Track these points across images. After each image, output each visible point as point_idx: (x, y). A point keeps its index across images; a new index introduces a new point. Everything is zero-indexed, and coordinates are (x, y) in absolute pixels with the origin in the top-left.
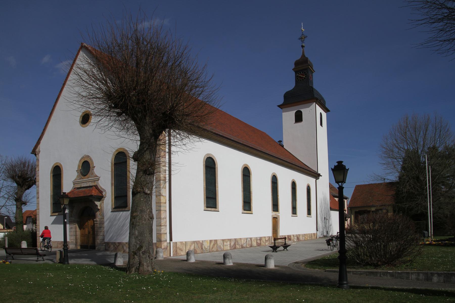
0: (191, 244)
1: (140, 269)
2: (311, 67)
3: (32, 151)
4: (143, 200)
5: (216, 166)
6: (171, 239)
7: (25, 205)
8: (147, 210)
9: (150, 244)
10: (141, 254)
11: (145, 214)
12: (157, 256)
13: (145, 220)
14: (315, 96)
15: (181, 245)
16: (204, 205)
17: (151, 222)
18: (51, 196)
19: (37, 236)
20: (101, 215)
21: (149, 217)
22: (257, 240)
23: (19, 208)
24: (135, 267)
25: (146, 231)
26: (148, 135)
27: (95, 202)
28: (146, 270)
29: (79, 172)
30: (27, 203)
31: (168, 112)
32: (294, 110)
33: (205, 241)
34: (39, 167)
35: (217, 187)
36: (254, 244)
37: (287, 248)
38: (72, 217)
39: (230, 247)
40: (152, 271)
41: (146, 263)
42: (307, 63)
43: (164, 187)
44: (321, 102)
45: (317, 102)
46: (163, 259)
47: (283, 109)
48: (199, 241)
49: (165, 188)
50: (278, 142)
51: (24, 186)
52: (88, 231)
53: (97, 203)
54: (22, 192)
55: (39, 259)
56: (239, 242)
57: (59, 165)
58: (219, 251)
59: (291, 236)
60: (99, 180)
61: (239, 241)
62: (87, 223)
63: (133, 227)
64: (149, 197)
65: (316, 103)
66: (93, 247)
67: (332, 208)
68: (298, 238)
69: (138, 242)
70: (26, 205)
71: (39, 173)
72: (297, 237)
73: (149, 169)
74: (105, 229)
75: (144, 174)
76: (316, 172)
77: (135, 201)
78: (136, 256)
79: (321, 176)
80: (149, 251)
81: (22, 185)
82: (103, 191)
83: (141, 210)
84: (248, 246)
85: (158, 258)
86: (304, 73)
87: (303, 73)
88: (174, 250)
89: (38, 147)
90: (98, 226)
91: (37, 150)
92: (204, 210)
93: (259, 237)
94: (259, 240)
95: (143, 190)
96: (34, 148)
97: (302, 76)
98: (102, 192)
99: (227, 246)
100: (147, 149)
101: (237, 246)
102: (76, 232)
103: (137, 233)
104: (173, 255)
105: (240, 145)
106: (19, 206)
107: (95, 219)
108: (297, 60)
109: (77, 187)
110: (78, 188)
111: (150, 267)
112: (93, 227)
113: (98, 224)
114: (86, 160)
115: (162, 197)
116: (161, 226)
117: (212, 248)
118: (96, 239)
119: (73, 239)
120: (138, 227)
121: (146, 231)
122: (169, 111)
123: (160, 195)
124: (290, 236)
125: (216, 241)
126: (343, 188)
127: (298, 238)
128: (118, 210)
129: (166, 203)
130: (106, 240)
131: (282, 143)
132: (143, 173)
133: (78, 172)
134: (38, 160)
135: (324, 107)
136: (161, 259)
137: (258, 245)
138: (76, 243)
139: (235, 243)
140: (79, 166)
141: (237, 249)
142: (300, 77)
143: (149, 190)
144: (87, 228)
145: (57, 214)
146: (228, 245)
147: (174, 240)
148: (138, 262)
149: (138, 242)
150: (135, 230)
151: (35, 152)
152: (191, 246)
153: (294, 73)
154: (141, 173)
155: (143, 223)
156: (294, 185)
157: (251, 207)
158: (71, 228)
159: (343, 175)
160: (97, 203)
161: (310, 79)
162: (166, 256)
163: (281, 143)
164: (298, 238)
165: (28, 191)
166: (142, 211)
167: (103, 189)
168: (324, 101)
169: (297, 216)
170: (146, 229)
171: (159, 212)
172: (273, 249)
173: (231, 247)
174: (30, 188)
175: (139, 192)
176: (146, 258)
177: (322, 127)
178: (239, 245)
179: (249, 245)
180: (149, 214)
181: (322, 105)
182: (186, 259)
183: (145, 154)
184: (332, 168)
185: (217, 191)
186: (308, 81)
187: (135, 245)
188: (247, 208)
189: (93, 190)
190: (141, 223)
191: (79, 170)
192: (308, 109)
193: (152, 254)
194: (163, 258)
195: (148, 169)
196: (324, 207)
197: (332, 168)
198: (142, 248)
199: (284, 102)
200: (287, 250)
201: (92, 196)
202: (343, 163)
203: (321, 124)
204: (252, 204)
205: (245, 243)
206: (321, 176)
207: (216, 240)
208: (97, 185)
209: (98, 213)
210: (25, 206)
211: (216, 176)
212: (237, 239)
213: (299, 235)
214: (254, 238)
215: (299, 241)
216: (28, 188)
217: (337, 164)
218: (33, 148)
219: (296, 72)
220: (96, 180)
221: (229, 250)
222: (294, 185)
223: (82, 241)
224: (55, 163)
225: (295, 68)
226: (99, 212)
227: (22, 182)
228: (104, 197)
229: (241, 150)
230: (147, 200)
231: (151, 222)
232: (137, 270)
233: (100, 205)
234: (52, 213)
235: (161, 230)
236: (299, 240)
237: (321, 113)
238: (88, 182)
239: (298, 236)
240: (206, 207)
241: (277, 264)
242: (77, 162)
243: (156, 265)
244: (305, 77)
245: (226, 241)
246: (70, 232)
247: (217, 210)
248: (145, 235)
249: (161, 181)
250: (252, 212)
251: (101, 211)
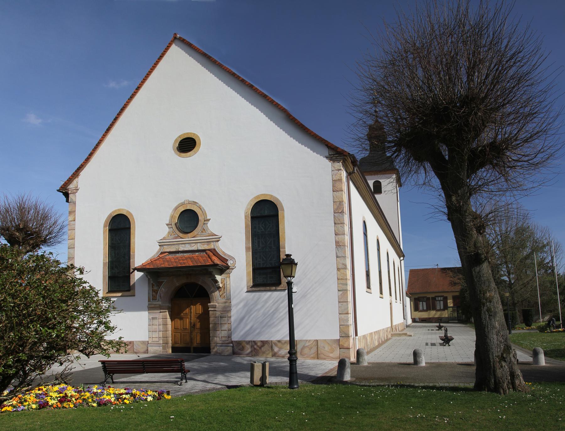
6: (356, 335)
18: (104, 264)
27: (216, 276)
52: (190, 323)
53: (218, 278)
60: (218, 241)
62: (187, 310)
74: (232, 319)
82: (228, 259)
91: (71, 186)
102: (165, 324)
112: (205, 317)
123: (345, 267)
126: (292, 283)
128: (258, 289)
130: (235, 337)
133: (170, 226)
140: (172, 217)
145: (120, 294)
159: (291, 268)
167: (229, 256)
191: (173, 224)
202: (292, 257)
208: (215, 249)
218: (62, 183)
223: (174, 342)
234: (107, 293)
238: (194, 244)
242: (170, 211)
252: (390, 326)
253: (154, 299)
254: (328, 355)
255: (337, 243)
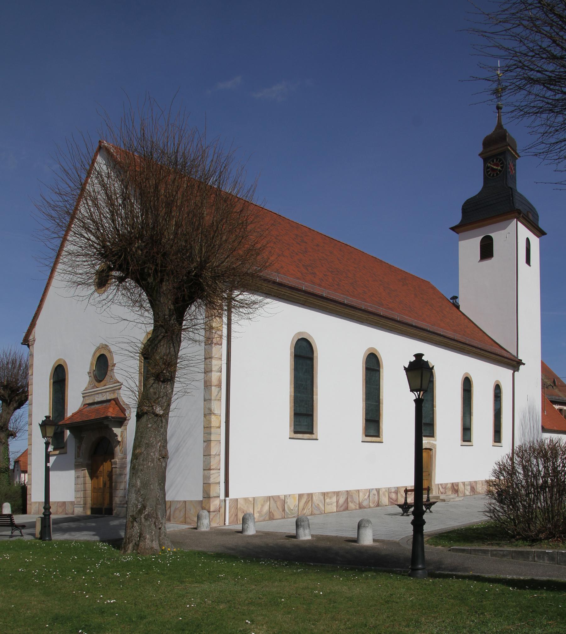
0: (264, 502)
1: (140, 545)
2: (511, 148)
3: (23, 339)
4: (151, 427)
5: (315, 355)
6: (227, 495)
7: (13, 438)
8: (156, 444)
9: (159, 502)
10: (143, 520)
11: (153, 450)
12: (199, 524)
13: (153, 461)
14: (517, 206)
15: (246, 504)
16: (290, 428)
17: (163, 464)
19: (28, 493)
20: (123, 451)
21: (160, 455)
22: (391, 492)
23: (4, 443)
24: (134, 542)
25: (154, 479)
26: (167, 312)
27: (114, 429)
28: (148, 547)
29: (92, 375)
30: (17, 434)
31: (193, 272)
32: (481, 236)
33: (290, 495)
34: (33, 369)
35: (314, 393)
36: (385, 500)
37: (430, 507)
38: (79, 457)
39: (337, 506)
40: (158, 548)
41: (150, 535)
42: (505, 139)
43: (218, 398)
44: (529, 218)
45: (519, 217)
46: (208, 530)
47: (459, 234)
48: (279, 497)
49: (220, 400)
50: (451, 299)
51: (12, 403)
52: (103, 481)
53: (117, 431)
54: (8, 413)
55: (14, 534)
56: (355, 496)
57: (62, 364)
58: (315, 514)
59: (458, 485)
60: (120, 389)
61: (354, 495)
63: (133, 473)
64: (162, 421)
65: (518, 219)
66: (109, 511)
67: (546, 427)
68: (474, 488)
69: (140, 499)
70: (14, 437)
71: (32, 379)
72: (471, 487)
73: (164, 373)
75: (157, 382)
76: (514, 356)
77: (140, 429)
78: (135, 524)
79: (524, 364)
80: (157, 515)
81: (9, 401)
82: (126, 408)
83: (147, 444)
84: (371, 505)
85: (200, 529)
86: (499, 161)
87: (497, 161)
88: (233, 514)
89: (32, 331)
90: (117, 473)
91: (31, 337)
92: (290, 438)
93: (395, 487)
94: (394, 492)
95: (153, 408)
96: (26, 335)
97: (496, 168)
98: (125, 410)
99: (331, 504)
100: (164, 337)
101: (351, 505)
102: (85, 484)
103: (139, 484)
104: (229, 523)
105: (360, 312)
106: (3, 440)
107: (113, 460)
108: (487, 137)
109: (88, 403)
110: (90, 404)
111: (156, 542)
112: (110, 475)
113: (118, 469)
114: (102, 353)
115: (213, 417)
116: (210, 469)
117: (303, 509)
118: (113, 496)
119: (79, 498)
120: (141, 473)
121: (154, 479)
122: (194, 270)
124: (457, 485)
125: (310, 496)
127: (473, 489)
129: (219, 427)
131: (457, 300)
132: (154, 379)
134: (32, 355)
135: (534, 227)
136: (206, 529)
137: (392, 503)
138: (85, 504)
139: (347, 498)
140: (92, 364)
141: (350, 510)
142: (493, 169)
143: (162, 408)
144: (102, 476)
145: (57, 452)
146: (333, 503)
147: (232, 495)
148: (138, 534)
149: (140, 499)
150: (136, 478)
151: (28, 341)
152: (263, 506)
153: (481, 161)
154: (151, 381)
155: (149, 467)
156: (467, 384)
157: (381, 430)
158: (77, 478)
160: (117, 431)
161: (509, 172)
162: (218, 525)
163: (456, 301)
164: (473, 489)
165: (18, 412)
166: (148, 445)
168: (536, 216)
169: (472, 446)
170: (154, 476)
171: (207, 444)
172: (402, 509)
173: (339, 508)
174: (22, 405)
175: (146, 413)
176: (150, 527)
177: (530, 265)
178: (355, 502)
179: (374, 503)
180: (160, 451)
181: (530, 223)
182: (242, 529)
183: (159, 345)
184: (405, 367)
185: (315, 402)
186: (506, 176)
187: (135, 504)
188: (372, 432)
189: (111, 407)
190: (145, 466)
191: (92, 371)
192: (502, 232)
193: (160, 519)
194: (209, 529)
195: (162, 372)
196: (529, 426)
197: (405, 367)
198: (145, 509)
199: (462, 221)
200: (431, 512)
201: (107, 418)
202: (423, 358)
203: (528, 261)
204: (382, 424)
205: (366, 500)
206: (524, 364)
207: (310, 494)
209: (118, 449)
210: (14, 439)
211: (314, 373)
212: (350, 491)
213: (476, 482)
214: (384, 490)
215: (475, 494)
216: (19, 407)
217: (414, 359)
218: (24, 334)
219: (485, 160)
220: (117, 389)
221: (335, 512)
222: (467, 384)
223: (93, 504)
224: (57, 361)
225: (483, 151)
226: (119, 447)
227: (9, 397)
228: (127, 419)
229: (363, 322)
230: (158, 426)
231: (164, 464)
232: (136, 548)
233: (122, 432)
235: (209, 478)
236: (475, 493)
237: (528, 240)
238: (105, 394)
239: (474, 484)
240: (293, 433)
241: (377, 538)
243: (167, 539)
244: (501, 170)
245: (330, 495)
246: (75, 484)
247: (313, 436)
248: (152, 486)
249: (213, 388)
250: (382, 440)
251: (122, 444)
252: (410, 483)
253: (78, 457)
254: (192, 519)
255: (205, 382)
